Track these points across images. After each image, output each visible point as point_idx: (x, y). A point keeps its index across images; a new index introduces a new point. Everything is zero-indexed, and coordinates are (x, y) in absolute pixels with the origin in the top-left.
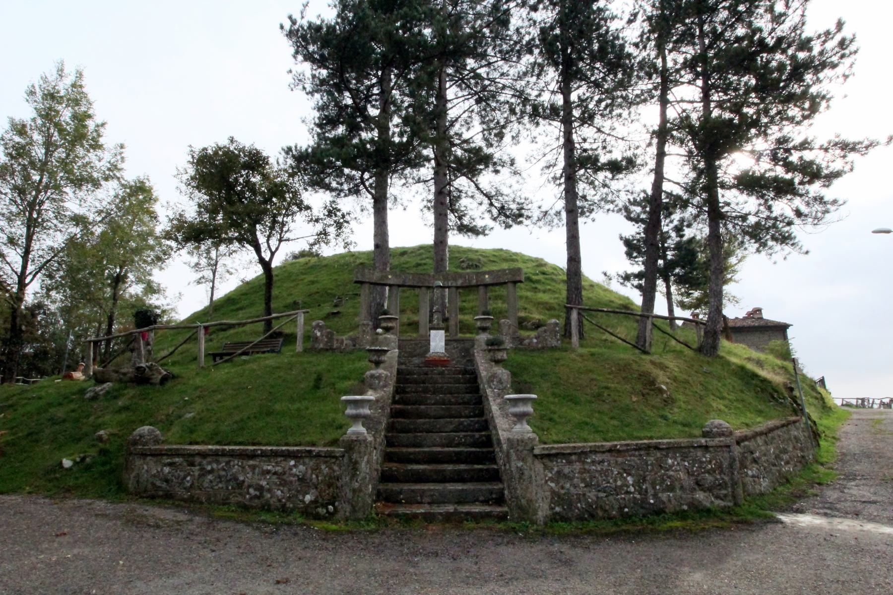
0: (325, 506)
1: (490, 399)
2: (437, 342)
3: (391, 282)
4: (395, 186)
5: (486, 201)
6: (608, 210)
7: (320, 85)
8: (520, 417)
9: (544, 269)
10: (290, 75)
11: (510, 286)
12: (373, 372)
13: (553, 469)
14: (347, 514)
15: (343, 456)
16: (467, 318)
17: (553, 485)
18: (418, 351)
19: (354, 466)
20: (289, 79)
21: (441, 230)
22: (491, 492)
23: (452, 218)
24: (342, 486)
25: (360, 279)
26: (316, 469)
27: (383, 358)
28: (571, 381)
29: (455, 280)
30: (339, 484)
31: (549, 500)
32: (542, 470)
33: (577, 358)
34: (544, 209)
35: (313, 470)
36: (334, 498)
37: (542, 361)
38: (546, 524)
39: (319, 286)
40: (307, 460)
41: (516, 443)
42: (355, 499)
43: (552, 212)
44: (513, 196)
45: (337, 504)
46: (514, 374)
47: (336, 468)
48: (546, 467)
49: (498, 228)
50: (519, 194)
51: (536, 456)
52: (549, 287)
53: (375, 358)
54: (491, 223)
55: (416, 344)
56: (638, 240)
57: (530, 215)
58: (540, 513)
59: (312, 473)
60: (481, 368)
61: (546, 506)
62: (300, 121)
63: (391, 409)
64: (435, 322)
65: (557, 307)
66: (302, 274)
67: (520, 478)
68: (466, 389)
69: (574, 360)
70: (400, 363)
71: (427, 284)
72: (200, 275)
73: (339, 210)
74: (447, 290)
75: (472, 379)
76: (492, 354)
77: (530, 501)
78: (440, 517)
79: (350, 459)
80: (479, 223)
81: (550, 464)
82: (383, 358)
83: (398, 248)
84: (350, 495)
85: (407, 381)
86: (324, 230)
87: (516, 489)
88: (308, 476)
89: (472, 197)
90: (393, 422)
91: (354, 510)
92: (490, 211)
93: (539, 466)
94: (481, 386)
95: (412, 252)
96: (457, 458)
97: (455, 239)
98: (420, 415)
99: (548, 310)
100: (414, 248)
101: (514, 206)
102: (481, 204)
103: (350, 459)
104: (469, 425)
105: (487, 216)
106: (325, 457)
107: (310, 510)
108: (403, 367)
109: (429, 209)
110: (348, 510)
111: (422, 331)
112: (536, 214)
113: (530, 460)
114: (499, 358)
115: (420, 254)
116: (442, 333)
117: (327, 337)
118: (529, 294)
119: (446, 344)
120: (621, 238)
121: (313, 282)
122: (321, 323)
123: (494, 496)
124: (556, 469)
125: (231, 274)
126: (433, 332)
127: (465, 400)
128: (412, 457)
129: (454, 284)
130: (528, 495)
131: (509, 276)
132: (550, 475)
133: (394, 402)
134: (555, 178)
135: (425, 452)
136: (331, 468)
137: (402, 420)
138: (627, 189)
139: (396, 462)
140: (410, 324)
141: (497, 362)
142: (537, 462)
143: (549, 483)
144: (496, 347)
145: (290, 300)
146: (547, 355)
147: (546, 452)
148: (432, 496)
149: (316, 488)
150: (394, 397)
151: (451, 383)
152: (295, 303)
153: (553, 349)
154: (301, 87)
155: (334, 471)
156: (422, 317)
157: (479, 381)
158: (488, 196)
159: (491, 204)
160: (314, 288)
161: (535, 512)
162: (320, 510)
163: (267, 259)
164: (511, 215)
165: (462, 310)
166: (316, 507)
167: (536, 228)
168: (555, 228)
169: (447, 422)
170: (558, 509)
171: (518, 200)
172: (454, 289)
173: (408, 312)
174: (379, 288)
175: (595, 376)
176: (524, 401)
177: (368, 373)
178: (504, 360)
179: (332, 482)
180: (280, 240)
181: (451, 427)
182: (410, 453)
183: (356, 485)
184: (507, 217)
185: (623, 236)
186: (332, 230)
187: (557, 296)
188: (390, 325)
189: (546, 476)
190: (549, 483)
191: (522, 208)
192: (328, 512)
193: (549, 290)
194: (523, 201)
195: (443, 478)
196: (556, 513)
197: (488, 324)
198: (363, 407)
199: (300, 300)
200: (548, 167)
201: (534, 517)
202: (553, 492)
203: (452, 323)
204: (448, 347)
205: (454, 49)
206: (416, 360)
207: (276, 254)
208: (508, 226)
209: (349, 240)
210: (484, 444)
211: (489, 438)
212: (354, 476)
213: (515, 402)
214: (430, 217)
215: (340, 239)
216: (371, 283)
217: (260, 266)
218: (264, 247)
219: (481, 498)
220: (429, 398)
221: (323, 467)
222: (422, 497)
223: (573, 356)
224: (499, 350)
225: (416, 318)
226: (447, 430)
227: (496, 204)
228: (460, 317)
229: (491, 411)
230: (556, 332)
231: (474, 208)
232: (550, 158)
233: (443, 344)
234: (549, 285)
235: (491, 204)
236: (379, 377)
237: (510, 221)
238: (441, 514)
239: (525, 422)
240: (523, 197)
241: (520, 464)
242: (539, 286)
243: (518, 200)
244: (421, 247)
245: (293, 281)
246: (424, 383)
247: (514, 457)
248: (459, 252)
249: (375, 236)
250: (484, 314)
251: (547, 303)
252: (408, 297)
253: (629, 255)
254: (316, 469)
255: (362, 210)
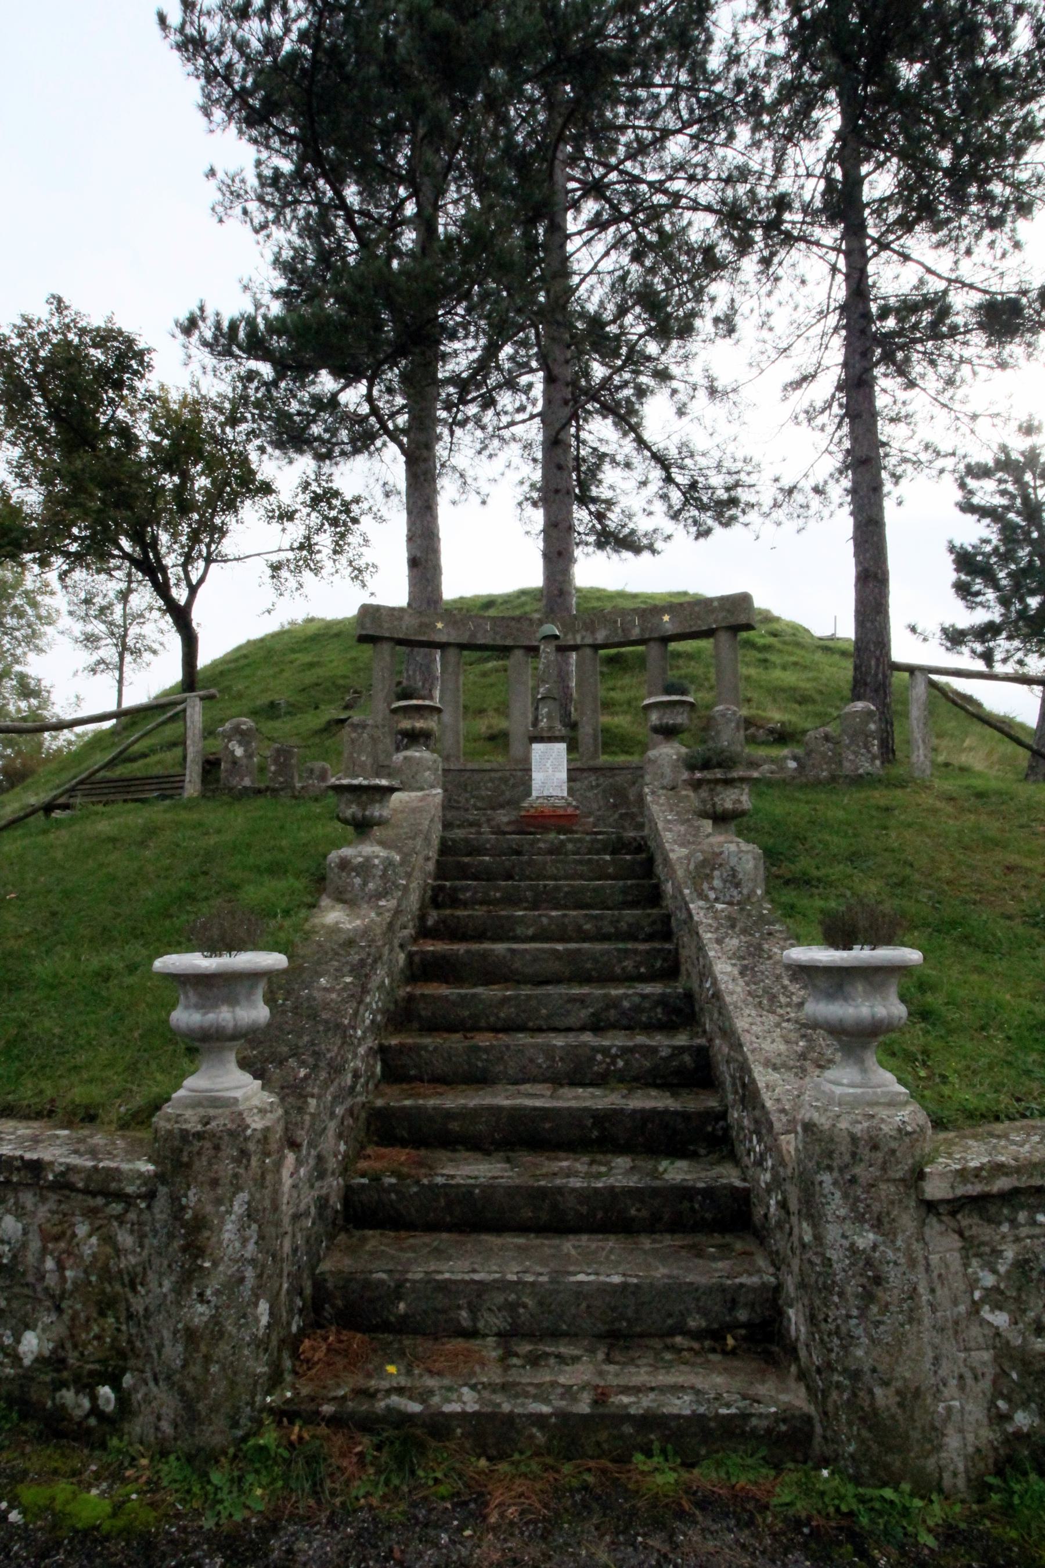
0: (87, 1385)
1: (707, 936)
2: (549, 770)
3: (444, 639)
4: (459, 450)
5: (656, 474)
6: (942, 471)
7: (278, 191)
8: (855, 1039)
9: (775, 626)
10: (213, 183)
11: (724, 637)
12: (347, 852)
13: (997, 1253)
14: (166, 1426)
15: (151, 1196)
16: (621, 721)
17: (1000, 1319)
18: (508, 795)
19: (193, 1237)
20: (210, 191)
21: (558, 554)
22: (731, 1297)
23: (581, 516)
24: (148, 1314)
25: (371, 632)
26: (57, 1236)
27: (376, 811)
28: (946, 873)
29: (591, 627)
30: (138, 1305)
31: (986, 1384)
32: (955, 1259)
33: (939, 804)
34: (786, 483)
35: (47, 1237)
36: (122, 1355)
37: (841, 814)
38: (980, 1489)
39: (320, 671)
40: (28, 1199)
41: (844, 1147)
42: (196, 1370)
43: (807, 485)
44: (716, 454)
45: (128, 1380)
46: (771, 856)
47: (125, 1239)
48: (970, 1247)
49: (681, 534)
50: (731, 448)
51: (930, 1207)
52: (794, 659)
53: (351, 810)
54: (669, 526)
55: (504, 780)
56: (988, 556)
57: (753, 500)
58: (953, 1442)
59: (44, 1251)
60: (667, 836)
61: (976, 1411)
62: (239, 288)
63: (410, 956)
64: (544, 723)
65: (817, 697)
66: (293, 651)
67: (868, 1297)
68: (625, 891)
69: (934, 811)
70: (447, 825)
71: (526, 643)
72: (96, 657)
73: (336, 494)
74: (574, 655)
75: (639, 865)
76: (704, 793)
77: (910, 1397)
78: (540, 1437)
79: (178, 1210)
80: (642, 525)
81: (984, 1232)
82: (376, 811)
83: (478, 597)
84: (174, 1352)
85: (464, 872)
86: (308, 538)
87: (848, 1341)
88: (31, 1259)
89: (628, 465)
90: (410, 998)
91: (191, 1416)
92: (665, 497)
93: (943, 1246)
94: (669, 887)
95: (505, 602)
96: (599, 1136)
97: (595, 571)
98: (492, 973)
99: (800, 703)
100: (509, 596)
101: (717, 480)
102: (644, 483)
103: (178, 1210)
104: (637, 1009)
105: (659, 507)
106: (86, 1191)
107: (34, 1394)
108: (459, 833)
109: (535, 504)
110: (168, 1412)
111: (516, 748)
112: (767, 494)
113: (907, 1221)
114: (729, 805)
115: (523, 604)
116: (560, 748)
117: (276, 761)
118: (752, 671)
119: (570, 779)
120: (952, 549)
121: (311, 665)
122: (247, 723)
123: (742, 1315)
124: (1010, 1253)
125: (155, 652)
126: (537, 748)
127: (623, 925)
128: (454, 1126)
129: (589, 641)
130: (904, 1371)
131: (722, 615)
132: (989, 1280)
133: (424, 932)
134: (811, 415)
135: (496, 1111)
136: (108, 1239)
137: (444, 990)
138: (994, 410)
139: (403, 1143)
140: (492, 738)
141: (721, 819)
142: (934, 1227)
143: (986, 1313)
144: (719, 774)
145: (263, 700)
146: (852, 799)
147: (974, 1189)
148: (511, 1307)
149: (59, 1310)
150: (422, 918)
151: (582, 877)
152: (273, 705)
153: (858, 781)
154: (238, 210)
155: (118, 1252)
156: (518, 723)
157: (660, 869)
158: (660, 459)
159: (669, 480)
160: (310, 677)
161: (934, 1436)
162: (68, 1396)
163: (182, 602)
164: (711, 505)
165: (607, 706)
166: (59, 1385)
167: (769, 526)
168: (812, 523)
169: (572, 1000)
170: (1023, 1420)
171: (727, 464)
172: (588, 651)
173: (491, 713)
174: (420, 653)
175: (1013, 858)
176: (873, 976)
177: (334, 856)
178: (743, 813)
179: (109, 1292)
180: (209, 560)
181: (584, 1013)
182: (449, 1115)
183: (200, 1313)
184: (703, 508)
185: (957, 544)
186: (325, 541)
187: (811, 675)
188: (419, 724)
189: (973, 1283)
190: (986, 1313)
191: (737, 485)
192: (95, 1410)
193: (795, 664)
194: (739, 465)
195: (552, 1217)
196: (1019, 1436)
197: (680, 718)
198: (232, 1001)
199: (281, 699)
200: (797, 385)
201: (931, 1463)
202: (1004, 1351)
203: (586, 731)
204: (577, 785)
205: (588, 78)
206: (503, 817)
207: (201, 592)
208: (704, 533)
209: (361, 563)
210: (697, 1095)
211: (703, 1057)
212: (189, 1276)
213: (836, 980)
214: (537, 517)
215: (343, 559)
216: (400, 642)
217: (168, 618)
218: (174, 573)
219: (694, 1322)
220: (521, 920)
221: (82, 1230)
222: (474, 1311)
223: (927, 800)
224: (728, 782)
225: (503, 724)
226: (572, 1021)
227: (679, 479)
228: (605, 719)
229: (706, 972)
230: (868, 735)
231: (629, 491)
232: (803, 357)
233: (563, 775)
234: (791, 654)
235: (669, 480)
236: (365, 869)
237: (707, 519)
238: (539, 1420)
239: (871, 1059)
240: (740, 456)
241: (865, 1239)
242: (773, 657)
243: (727, 464)
244: (523, 593)
245: (276, 664)
246: (510, 877)
247: (836, 1205)
248: (599, 599)
249: (410, 539)
250: (668, 691)
251: (794, 689)
252: (492, 685)
253: (963, 590)
254: (57, 1236)
255: (387, 495)
